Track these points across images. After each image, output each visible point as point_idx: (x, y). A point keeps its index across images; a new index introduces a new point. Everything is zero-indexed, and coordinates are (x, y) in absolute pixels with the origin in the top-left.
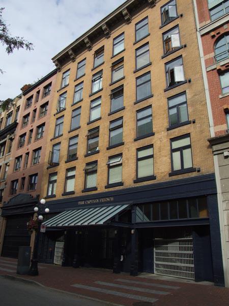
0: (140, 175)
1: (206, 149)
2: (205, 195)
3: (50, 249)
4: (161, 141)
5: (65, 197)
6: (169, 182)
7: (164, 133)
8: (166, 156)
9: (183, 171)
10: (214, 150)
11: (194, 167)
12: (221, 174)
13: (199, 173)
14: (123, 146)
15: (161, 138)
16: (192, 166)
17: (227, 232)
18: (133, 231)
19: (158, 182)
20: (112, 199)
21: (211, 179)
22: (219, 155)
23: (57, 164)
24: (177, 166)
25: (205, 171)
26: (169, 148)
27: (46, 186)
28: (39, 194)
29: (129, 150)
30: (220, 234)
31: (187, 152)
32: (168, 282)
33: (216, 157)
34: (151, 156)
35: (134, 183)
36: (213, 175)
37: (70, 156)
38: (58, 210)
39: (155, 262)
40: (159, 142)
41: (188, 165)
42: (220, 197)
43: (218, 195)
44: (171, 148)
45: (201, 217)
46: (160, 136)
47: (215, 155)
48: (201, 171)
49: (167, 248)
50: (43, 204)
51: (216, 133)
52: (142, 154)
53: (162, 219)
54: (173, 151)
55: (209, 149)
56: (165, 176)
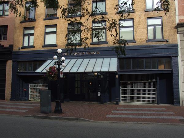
0: (47, 43)
1: (173, 29)
2: (171, 56)
3: (25, 90)
4: (140, 18)
5: (43, 49)
6: (146, 46)
7: (142, 13)
8: (144, 29)
9: (29, 47)
10: (179, 30)
11: (57, 44)
12: (181, 45)
13: (167, 43)
14: (34, 22)
15: (140, 16)
16: (55, 44)
17: (183, 77)
18: (117, 76)
19: (138, 45)
20: (99, 53)
21: (175, 48)
22: (180, 34)
23: (34, 20)
24: (151, 37)
25: (171, 42)
26: (44, 31)
27: (21, 38)
28: (12, 44)
29: (40, 24)
30: (12, 83)
31: (32, 38)
32: (124, 105)
33: (178, 35)
34: (55, 33)
35: (91, 45)
36: (177, 45)
37: (48, 15)
38: (43, 59)
39: (121, 95)
40: (138, 18)
41: (31, 44)
42: (180, 59)
43: (179, 57)
44: (147, 24)
45: (159, 69)
46: (139, 14)
47: (178, 33)
48: (169, 42)
49: (132, 87)
50: (59, 53)
51: (179, 20)
52: (48, 30)
53: (133, 69)
54: (25, 35)
55: (175, 29)
56: (143, 41)
